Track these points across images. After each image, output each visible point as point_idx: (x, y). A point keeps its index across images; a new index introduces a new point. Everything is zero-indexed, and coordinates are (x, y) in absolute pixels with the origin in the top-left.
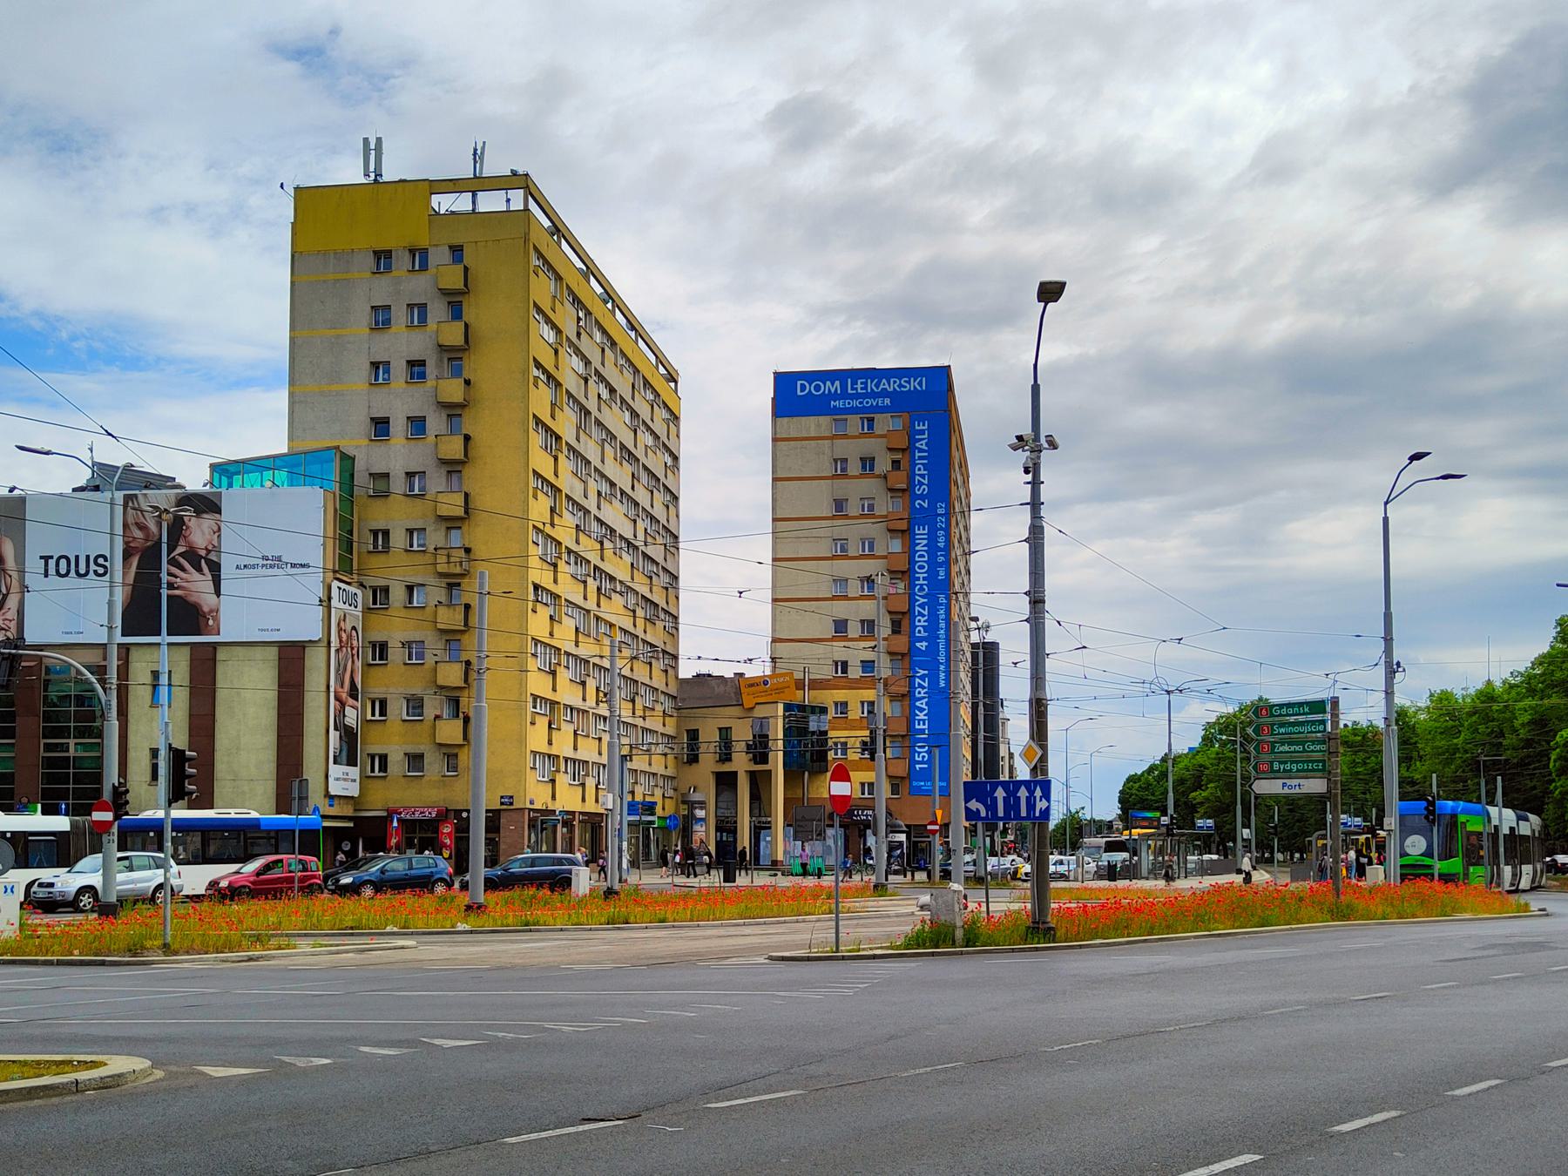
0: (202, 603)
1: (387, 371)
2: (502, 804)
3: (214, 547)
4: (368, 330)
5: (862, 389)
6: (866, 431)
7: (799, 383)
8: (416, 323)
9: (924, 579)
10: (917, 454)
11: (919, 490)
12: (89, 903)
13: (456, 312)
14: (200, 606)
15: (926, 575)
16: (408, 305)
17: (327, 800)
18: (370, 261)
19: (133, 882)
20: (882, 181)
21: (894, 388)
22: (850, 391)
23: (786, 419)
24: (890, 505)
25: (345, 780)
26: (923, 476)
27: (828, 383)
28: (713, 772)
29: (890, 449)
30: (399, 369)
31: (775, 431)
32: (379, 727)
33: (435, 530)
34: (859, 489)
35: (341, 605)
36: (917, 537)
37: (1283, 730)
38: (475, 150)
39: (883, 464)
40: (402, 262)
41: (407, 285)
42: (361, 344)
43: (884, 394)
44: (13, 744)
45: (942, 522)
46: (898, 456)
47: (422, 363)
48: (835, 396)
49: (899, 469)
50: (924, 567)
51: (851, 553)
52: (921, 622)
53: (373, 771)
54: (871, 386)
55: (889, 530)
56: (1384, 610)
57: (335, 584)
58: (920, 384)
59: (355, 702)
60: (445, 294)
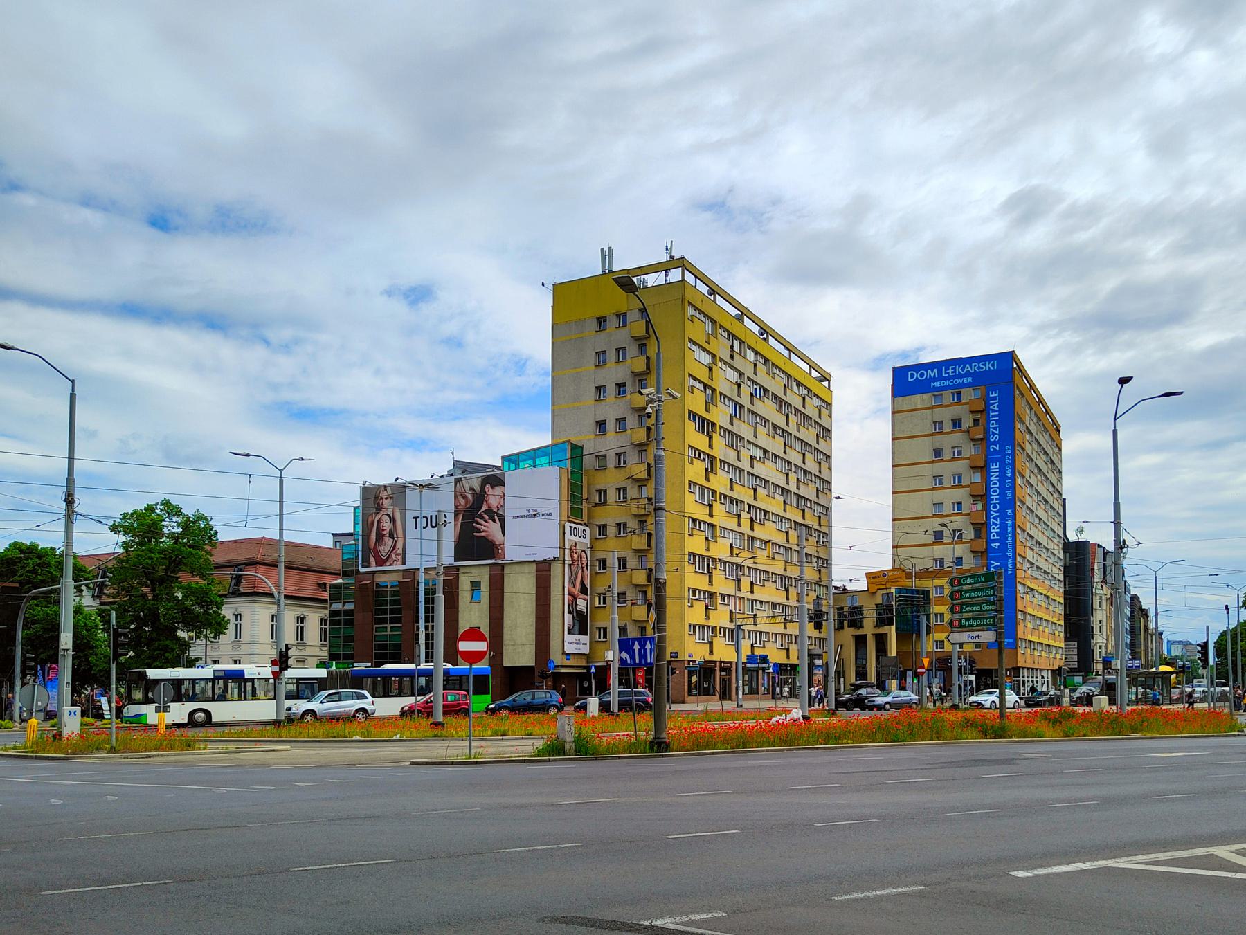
0: (495, 540)
1: (605, 392)
2: (671, 657)
3: (501, 506)
4: (594, 367)
5: (952, 372)
6: (955, 401)
7: (909, 373)
8: (621, 360)
9: (997, 499)
10: (991, 414)
11: (992, 438)
12: (363, 718)
13: (642, 347)
14: (494, 541)
15: (998, 497)
16: (616, 349)
17: (565, 656)
18: (595, 324)
19: (340, 707)
20: (1083, 236)
21: (975, 370)
22: (944, 375)
23: (901, 398)
24: (973, 450)
25: (578, 644)
26: (995, 429)
27: (929, 371)
28: (853, 635)
29: (972, 412)
30: (611, 389)
31: (893, 408)
32: (602, 610)
33: (632, 488)
34: (951, 441)
35: (573, 538)
36: (991, 471)
37: (967, 595)
38: (667, 246)
39: (967, 423)
40: (612, 322)
41: (617, 336)
42: (591, 375)
43: (968, 374)
44: (401, 627)
45: (1009, 459)
46: (978, 416)
47: (624, 385)
48: (934, 380)
49: (978, 425)
50: (996, 491)
51: (945, 486)
52: (995, 529)
53: (600, 638)
54: (958, 370)
55: (972, 468)
56: (1113, 501)
57: (568, 525)
58: (993, 365)
59: (585, 596)
60: (636, 340)
